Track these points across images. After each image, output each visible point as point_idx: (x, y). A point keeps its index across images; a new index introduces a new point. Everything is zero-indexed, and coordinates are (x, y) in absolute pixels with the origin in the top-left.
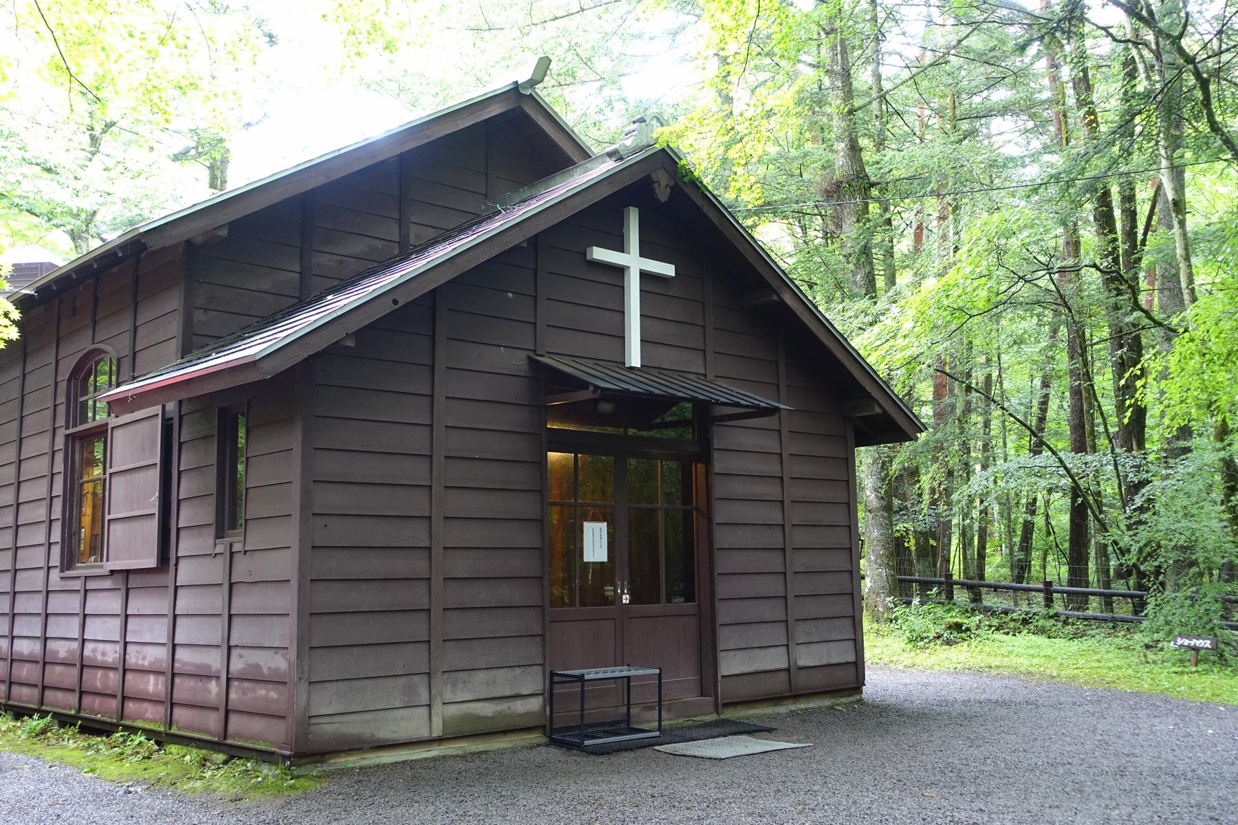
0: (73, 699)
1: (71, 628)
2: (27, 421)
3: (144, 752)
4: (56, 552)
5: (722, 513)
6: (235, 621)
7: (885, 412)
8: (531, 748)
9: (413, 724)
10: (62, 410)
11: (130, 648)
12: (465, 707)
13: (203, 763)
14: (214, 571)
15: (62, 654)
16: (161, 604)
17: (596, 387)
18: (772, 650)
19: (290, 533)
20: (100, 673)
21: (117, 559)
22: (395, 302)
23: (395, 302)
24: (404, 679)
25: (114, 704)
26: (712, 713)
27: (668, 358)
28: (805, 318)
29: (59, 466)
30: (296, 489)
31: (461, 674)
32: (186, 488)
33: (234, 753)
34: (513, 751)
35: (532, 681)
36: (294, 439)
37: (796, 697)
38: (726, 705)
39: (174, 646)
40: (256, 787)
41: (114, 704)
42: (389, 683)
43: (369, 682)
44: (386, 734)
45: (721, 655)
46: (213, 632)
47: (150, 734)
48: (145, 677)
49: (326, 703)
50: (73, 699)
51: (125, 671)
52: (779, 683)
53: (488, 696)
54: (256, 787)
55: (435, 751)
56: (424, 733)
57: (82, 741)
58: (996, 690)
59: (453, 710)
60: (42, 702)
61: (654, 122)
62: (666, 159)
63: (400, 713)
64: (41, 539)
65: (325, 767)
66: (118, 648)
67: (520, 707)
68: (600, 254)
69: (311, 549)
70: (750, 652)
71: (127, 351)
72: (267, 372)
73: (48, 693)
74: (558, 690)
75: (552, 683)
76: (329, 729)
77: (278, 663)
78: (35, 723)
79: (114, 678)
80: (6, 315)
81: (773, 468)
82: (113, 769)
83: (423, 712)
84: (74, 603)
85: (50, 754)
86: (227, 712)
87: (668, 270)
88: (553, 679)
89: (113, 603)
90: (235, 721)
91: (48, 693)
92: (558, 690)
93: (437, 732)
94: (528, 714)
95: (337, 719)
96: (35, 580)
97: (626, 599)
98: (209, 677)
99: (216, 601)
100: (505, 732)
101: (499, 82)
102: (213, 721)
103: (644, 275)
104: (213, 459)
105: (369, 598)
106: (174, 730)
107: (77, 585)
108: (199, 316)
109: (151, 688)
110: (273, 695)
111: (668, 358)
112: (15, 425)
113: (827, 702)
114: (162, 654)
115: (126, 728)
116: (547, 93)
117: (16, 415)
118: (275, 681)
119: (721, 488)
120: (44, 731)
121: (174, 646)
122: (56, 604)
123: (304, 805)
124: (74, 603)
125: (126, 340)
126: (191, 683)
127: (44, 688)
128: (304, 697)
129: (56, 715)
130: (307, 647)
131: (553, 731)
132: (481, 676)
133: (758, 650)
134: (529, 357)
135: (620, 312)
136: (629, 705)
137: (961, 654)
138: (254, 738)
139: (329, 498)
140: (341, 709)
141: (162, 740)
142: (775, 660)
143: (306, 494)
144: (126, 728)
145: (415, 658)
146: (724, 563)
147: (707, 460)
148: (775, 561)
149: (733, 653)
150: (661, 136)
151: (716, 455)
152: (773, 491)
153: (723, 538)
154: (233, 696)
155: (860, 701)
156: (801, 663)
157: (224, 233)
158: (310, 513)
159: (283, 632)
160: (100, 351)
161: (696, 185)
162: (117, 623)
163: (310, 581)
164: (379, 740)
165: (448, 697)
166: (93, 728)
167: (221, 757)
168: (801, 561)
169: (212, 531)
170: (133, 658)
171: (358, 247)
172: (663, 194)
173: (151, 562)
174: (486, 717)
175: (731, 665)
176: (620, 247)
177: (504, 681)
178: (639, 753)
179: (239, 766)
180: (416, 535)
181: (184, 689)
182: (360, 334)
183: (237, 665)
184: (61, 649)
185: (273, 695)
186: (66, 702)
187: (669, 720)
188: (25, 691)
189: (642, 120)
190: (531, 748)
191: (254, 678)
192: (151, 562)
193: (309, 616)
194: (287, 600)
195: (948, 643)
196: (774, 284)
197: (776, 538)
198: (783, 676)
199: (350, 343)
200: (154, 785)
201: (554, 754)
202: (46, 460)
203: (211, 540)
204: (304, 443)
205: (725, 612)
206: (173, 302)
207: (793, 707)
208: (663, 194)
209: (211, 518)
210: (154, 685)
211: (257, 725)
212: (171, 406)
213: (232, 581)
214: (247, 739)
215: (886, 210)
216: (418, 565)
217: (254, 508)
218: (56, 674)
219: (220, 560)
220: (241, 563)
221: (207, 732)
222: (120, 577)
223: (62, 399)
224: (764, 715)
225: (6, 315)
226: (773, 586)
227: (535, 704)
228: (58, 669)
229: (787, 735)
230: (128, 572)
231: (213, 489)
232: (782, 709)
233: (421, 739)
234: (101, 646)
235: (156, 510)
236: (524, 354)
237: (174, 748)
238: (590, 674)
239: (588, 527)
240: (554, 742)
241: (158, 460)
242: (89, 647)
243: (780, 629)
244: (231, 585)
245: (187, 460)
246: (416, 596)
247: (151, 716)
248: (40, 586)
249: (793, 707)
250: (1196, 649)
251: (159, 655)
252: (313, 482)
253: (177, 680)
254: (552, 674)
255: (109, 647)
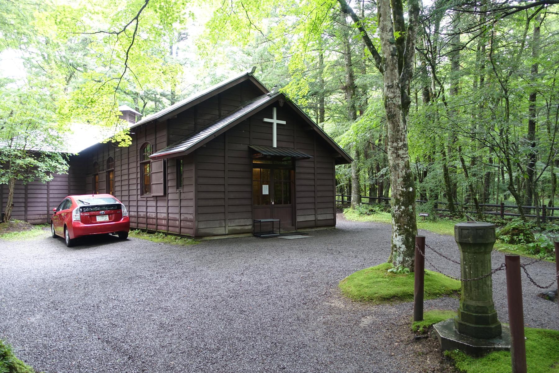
0: (145, 226)
1: (144, 209)
2: (130, 159)
3: (162, 237)
4: (139, 191)
5: (297, 183)
6: (182, 208)
7: (342, 156)
8: (249, 237)
9: (221, 231)
10: (139, 157)
11: (158, 214)
13: (176, 239)
14: (177, 196)
15: (142, 215)
16: (165, 204)
17: (263, 154)
19: (193, 188)
20: (151, 220)
21: (154, 193)
22: (215, 136)
23: (215, 136)
25: (155, 227)
27: (284, 144)
28: (320, 133)
29: (139, 170)
30: (194, 179)
32: (169, 177)
33: (182, 237)
34: (245, 237)
35: (249, 222)
36: (193, 168)
37: (317, 227)
38: (298, 228)
39: (168, 213)
40: (187, 243)
41: (155, 227)
42: (216, 221)
44: (215, 233)
45: (297, 217)
46: (177, 210)
47: (163, 233)
48: (162, 220)
49: (202, 226)
50: (145, 226)
51: (157, 219)
52: (313, 224)
54: (187, 243)
55: (226, 237)
56: (224, 233)
57: (148, 235)
58: (374, 226)
59: (230, 228)
60: (138, 226)
61: (280, 86)
62: (282, 96)
63: (218, 228)
64: (135, 188)
65: (202, 239)
66: (155, 214)
67: (246, 228)
68: (266, 120)
69: (197, 192)
71: (154, 144)
72: (186, 154)
73: (139, 224)
74: (256, 224)
75: (254, 222)
76: (203, 231)
77: (191, 217)
78: (137, 231)
79: (155, 221)
80: (129, 139)
81: (312, 171)
82: (156, 240)
83: (224, 228)
84: (144, 203)
85: (141, 238)
86: (181, 228)
87: (284, 123)
88: (254, 222)
89: (154, 203)
90: (182, 230)
91: (139, 224)
92: (256, 224)
93: (227, 233)
94: (248, 229)
96: (135, 198)
97: (273, 203)
98: (176, 220)
99: (177, 203)
100: (243, 233)
101: (244, 73)
102: (178, 230)
103: (277, 124)
104: (175, 171)
105: (211, 203)
106: (169, 232)
107: (145, 199)
108: (171, 136)
109: (163, 223)
110: (190, 224)
111: (284, 144)
112: (127, 159)
113: (325, 228)
114: (166, 215)
115: (158, 232)
116: (255, 75)
117: (127, 157)
118: (191, 221)
119: (297, 176)
120: (139, 233)
121: (168, 213)
122: (140, 203)
123: (197, 246)
124: (144, 203)
125: (154, 141)
126: (172, 221)
127: (138, 223)
128: (197, 224)
129: (141, 229)
130: (197, 213)
131: (254, 233)
132: (237, 221)
134: (248, 146)
135: (272, 134)
136: (273, 228)
137: (371, 218)
138: (187, 233)
139: (201, 181)
140: (205, 227)
141: (166, 234)
142: (312, 218)
143: (196, 180)
144: (158, 232)
146: (298, 195)
147: (295, 170)
148: (312, 194)
150: (281, 90)
151: (296, 168)
152: (312, 177)
153: (298, 188)
154: (182, 224)
155: (335, 228)
156: (319, 219)
157: (176, 117)
158: (197, 184)
159: (192, 210)
160: (148, 143)
161: (290, 102)
162: (155, 208)
163: (197, 199)
165: (229, 225)
166: (150, 232)
167: (179, 238)
168: (319, 194)
169: (176, 187)
170: (159, 216)
171: (208, 117)
172: (281, 105)
173: (162, 194)
175: (300, 219)
176: (272, 118)
177: (242, 222)
178: (273, 238)
179: (183, 239)
180: (222, 189)
181: (171, 223)
182: (207, 144)
183: (182, 218)
184: (142, 214)
185: (190, 224)
186: (144, 226)
188: (133, 224)
189: (276, 86)
190: (249, 237)
191: (186, 220)
192: (162, 194)
193: (197, 207)
194: (192, 203)
195: (369, 215)
196: (312, 125)
197: (312, 188)
198: (314, 222)
199: (205, 146)
200: (165, 243)
201: (254, 238)
202: (135, 169)
203: (175, 189)
204: (196, 169)
205: (298, 206)
206: (165, 133)
208: (281, 105)
209: (175, 185)
210: (164, 222)
211: (187, 230)
212: (166, 159)
214: (185, 233)
216: (222, 196)
217: (185, 182)
218: (141, 220)
219: (178, 194)
220: (182, 195)
221: (176, 232)
222: (155, 197)
223: (139, 154)
225: (129, 139)
226: (311, 200)
227: (250, 227)
228: (141, 219)
229: (311, 235)
230: (157, 196)
231: (176, 177)
232: (313, 230)
234: (151, 213)
235: (163, 182)
236: (247, 145)
237: (169, 236)
238: (262, 221)
239: (264, 186)
240: (254, 236)
241: (163, 170)
242: (148, 214)
243: (332, 209)
244: (180, 200)
245: (169, 171)
246: (221, 202)
247: (164, 229)
248: (136, 199)
250: (424, 216)
251: (165, 215)
252: (197, 177)
253: (169, 221)
254: (254, 220)
255: (153, 214)
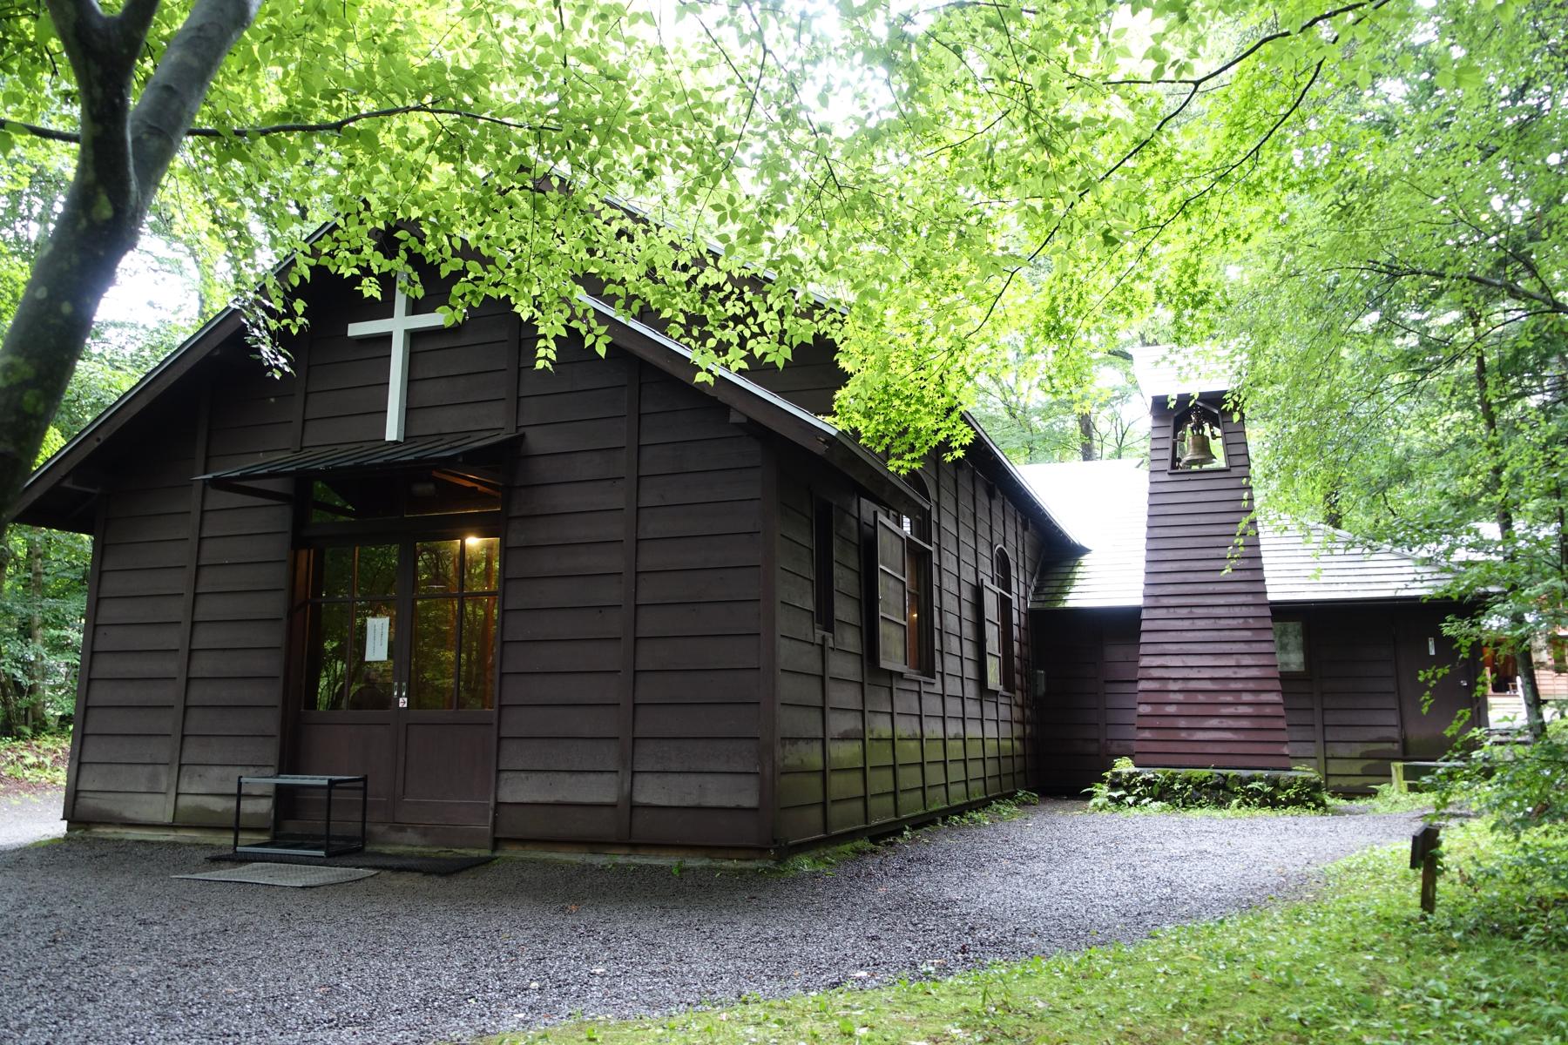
12: (199, 799)
18: (592, 777)
24: (151, 767)
26: (485, 848)
31: (198, 768)
37: (635, 846)
43: (124, 767)
44: (130, 814)
53: (220, 791)
55: (171, 836)
70: (552, 776)
95: (98, 795)
97: (403, 702)
133: (567, 776)
145: (163, 750)
149: (523, 775)
164: (125, 818)
174: (214, 812)
187: (424, 846)
207: (621, 860)
213: (193, 647)
215: (916, 89)
224: (568, 862)
232: (599, 860)
233: (424, 883)
249: (621, 860)
